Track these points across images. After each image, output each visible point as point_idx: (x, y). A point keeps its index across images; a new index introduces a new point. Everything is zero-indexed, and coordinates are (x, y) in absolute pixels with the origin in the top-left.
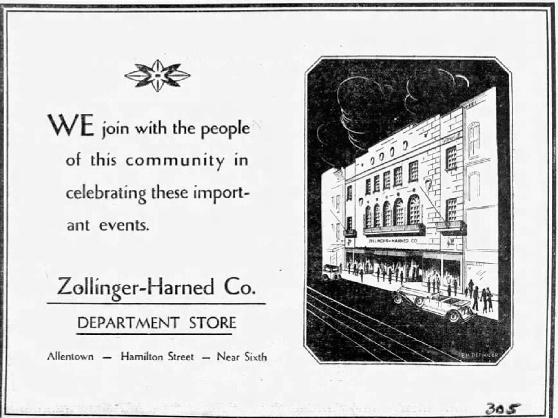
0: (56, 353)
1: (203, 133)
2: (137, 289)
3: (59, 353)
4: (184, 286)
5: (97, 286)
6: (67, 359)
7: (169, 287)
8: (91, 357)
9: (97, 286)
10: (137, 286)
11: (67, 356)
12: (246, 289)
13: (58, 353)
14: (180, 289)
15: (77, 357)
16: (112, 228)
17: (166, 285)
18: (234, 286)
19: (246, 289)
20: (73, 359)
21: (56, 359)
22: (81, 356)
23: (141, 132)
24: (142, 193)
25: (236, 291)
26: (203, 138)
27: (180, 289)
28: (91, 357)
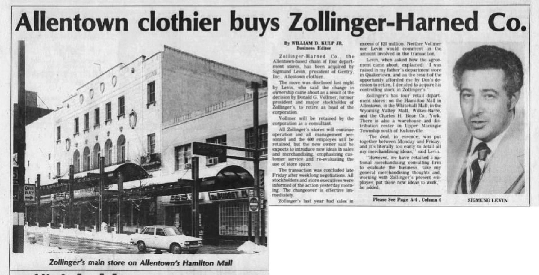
0: (36, 13)
1: (475, 20)
2: (384, 24)
3: (43, 13)
4: (439, 20)
5: (333, 20)
6: (62, 29)
7: (420, 21)
8: (122, 24)
9: (333, 20)
10: (385, 20)
11: (62, 21)
12: (514, 24)
13: (39, 16)
14: (435, 24)
15: (89, 25)
16: (500, 201)
17: (418, 19)
18: (499, 22)
19: (514, 24)
20: (78, 29)
21: (36, 29)
22: (99, 20)
23: (105, 28)
24: (357, 22)
25: (501, 27)
26: (475, 13)
27: (435, 24)
28: (122, 24)
